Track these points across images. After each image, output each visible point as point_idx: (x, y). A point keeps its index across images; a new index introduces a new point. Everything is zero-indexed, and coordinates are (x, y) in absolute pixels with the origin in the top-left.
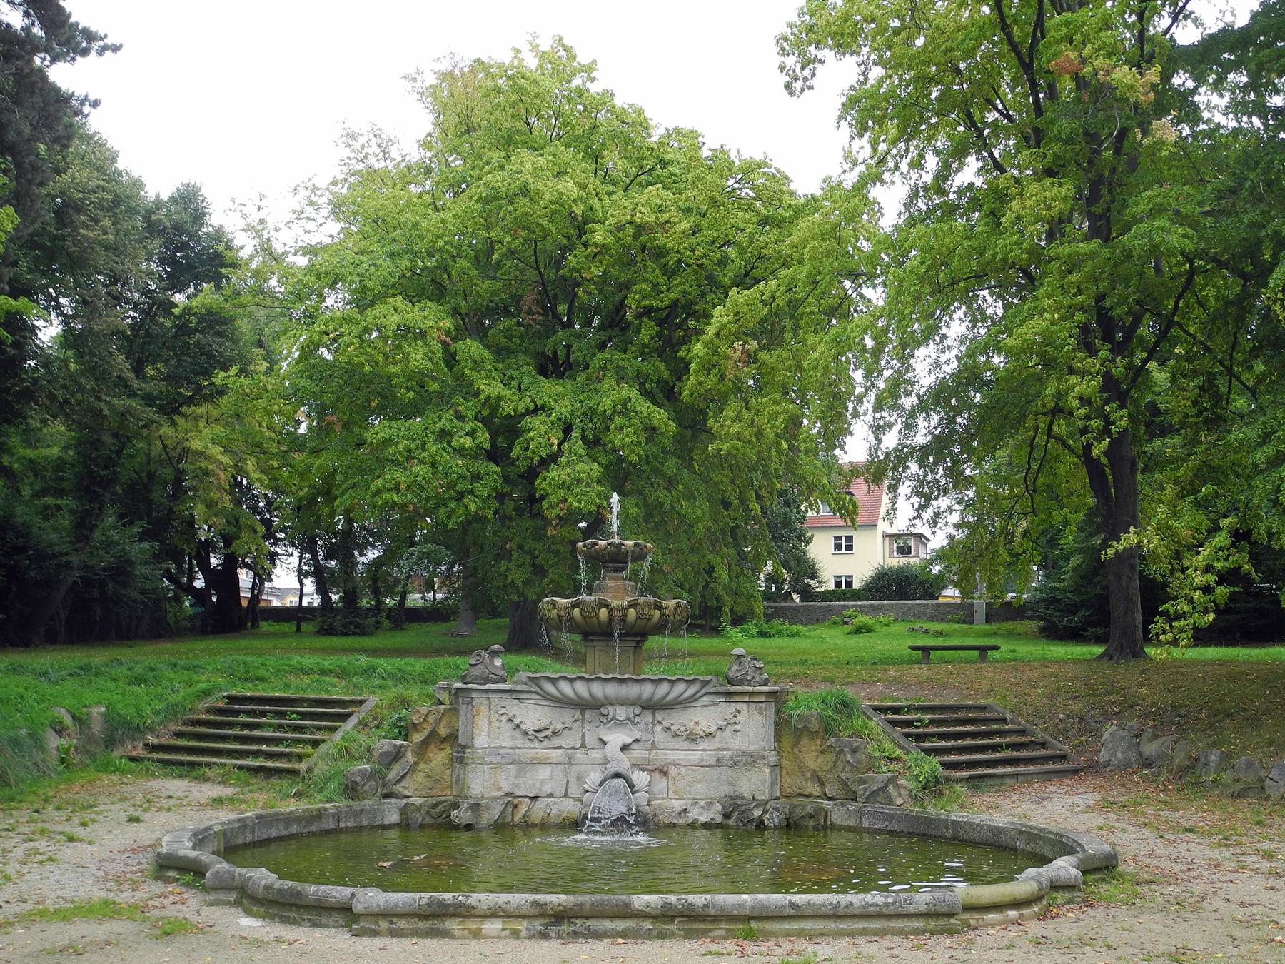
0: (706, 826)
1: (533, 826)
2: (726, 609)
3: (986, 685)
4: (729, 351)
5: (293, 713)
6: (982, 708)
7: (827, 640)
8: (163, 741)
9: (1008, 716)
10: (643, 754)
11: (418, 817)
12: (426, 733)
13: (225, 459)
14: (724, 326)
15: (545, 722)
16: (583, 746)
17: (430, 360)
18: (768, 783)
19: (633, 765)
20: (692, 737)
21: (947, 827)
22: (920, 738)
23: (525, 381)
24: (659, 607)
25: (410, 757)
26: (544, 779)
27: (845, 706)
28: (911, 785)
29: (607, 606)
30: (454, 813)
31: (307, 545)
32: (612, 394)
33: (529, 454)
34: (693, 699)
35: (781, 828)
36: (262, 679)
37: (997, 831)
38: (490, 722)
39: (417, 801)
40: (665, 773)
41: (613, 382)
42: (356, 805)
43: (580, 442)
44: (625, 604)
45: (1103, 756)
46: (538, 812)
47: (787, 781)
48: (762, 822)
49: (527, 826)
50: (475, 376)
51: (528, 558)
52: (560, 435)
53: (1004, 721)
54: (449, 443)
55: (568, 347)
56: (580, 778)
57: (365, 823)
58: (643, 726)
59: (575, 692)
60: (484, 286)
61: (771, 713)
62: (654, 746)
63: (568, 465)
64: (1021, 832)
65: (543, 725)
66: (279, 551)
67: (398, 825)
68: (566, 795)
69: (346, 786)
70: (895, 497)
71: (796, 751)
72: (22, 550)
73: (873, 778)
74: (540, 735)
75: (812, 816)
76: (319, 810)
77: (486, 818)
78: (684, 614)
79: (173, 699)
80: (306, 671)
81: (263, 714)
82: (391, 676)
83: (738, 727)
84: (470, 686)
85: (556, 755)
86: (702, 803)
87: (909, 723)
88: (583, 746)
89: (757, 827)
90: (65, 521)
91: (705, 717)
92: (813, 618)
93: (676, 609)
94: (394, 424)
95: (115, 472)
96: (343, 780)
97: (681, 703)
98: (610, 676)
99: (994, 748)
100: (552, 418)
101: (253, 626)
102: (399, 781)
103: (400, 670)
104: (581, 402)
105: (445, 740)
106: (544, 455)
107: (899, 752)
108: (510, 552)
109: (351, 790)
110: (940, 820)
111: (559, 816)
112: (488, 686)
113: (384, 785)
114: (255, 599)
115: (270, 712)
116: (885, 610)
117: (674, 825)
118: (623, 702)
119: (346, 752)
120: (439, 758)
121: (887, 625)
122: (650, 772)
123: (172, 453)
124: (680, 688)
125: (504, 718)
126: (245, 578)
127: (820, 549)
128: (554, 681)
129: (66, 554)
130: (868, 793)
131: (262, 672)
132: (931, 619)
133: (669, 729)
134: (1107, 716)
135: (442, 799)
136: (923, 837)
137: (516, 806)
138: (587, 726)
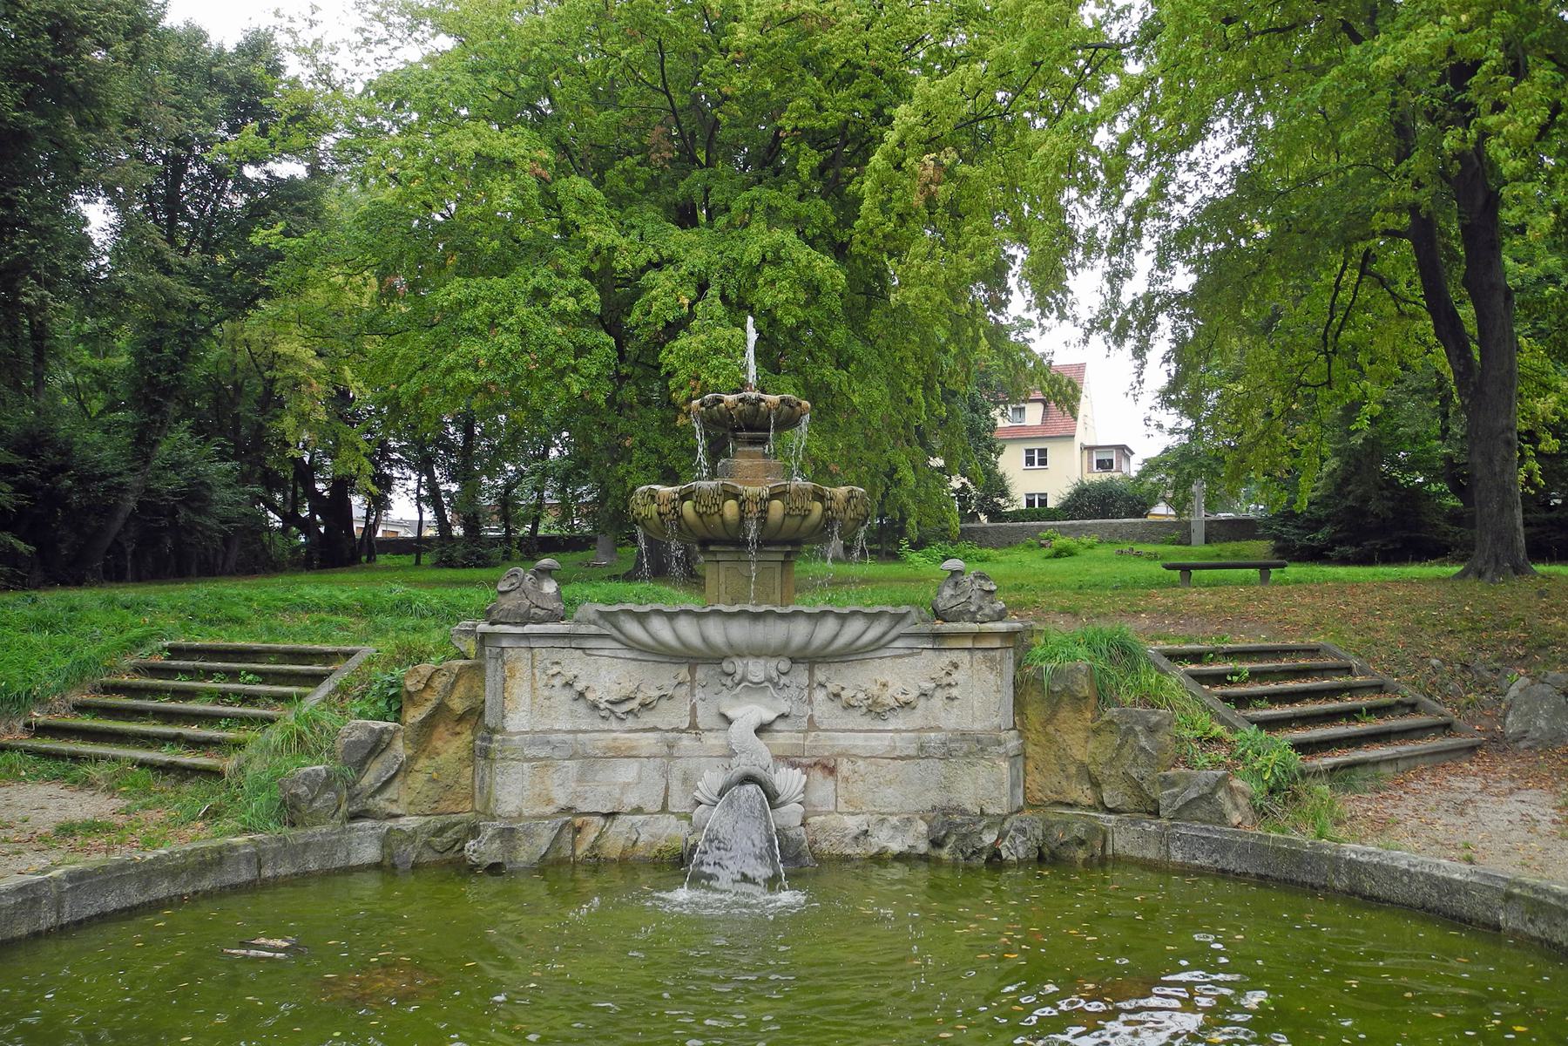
0: (900, 857)
1: (609, 861)
2: (912, 521)
3: (1307, 617)
4: (917, 167)
5: (249, 672)
6: (1313, 652)
7: (1018, 564)
8: (55, 720)
9: (1355, 662)
10: (796, 738)
11: (410, 853)
12: (426, 709)
13: (318, 365)
14: (911, 129)
15: (627, 688)
16: (693, 726)
17: (521, 197)
18: (1007, 785)
19: (777, 758)
20: (876, 710)
21: (1336, 871)
22: (1242, 701)
23: (649, 228)
24: (820, 497)
25: (400, 749)
26: (627, 782)
27: (1124, 652)
28: (1253, 788)
29: (736, 496)
30: (471, 844)
31: (424, 466)
32: (759, 240)
33: (651, 319)
34: (877, 645)
35: (1029, 862)
36: (238, 621)
37: (1449, 887)
38: (533, 689)
39: (409, 823)
40: (831, 771)
41: (763, 226)
42: (296, 835)
43: (718, 302)
44: (765, 493)
45: (1513, 725)
46: (616, 839)
47: (1035, 779)
48: (997, 854)
49: (597, 863)
50: (580, 220)
51: (655, 457)
52: (693, 293)
53: (1348, 670)
54: (545, 305)
55: (707, 190)
56: (688, 780)
57: (313, 866)
58: (793, 692)
59: (678, 637)
60: (600, 119)
61: (1009, 668)
62: (812, 725)
63: (702, 330)
64: (1509, 897)
66: (396, 474)
67: (377, 866)
68: (664, 809)
69: (283, 803)
70: (1142, 365)
71: (1050, 729)
72: (63, 469)
73: (1187, 777)
74: (619, 710)
75: (1081, 843)
76: (219, 850)
77: (526, 853)
78: (861, 509)
79: (90, 651)
80: (307, 608)
81: (209, 674)
82: (435, 613)
83: (954, 692)
84: (498, 628)
85: (648, 741)
86: (894, 820)
87: (1219, 679)
88: (693, 726)
89: (988, 861)
90: (123, 439)
91: (897, 675)
92: (1007, 541)
93: (848, 501)
94: (472, 282)
95: (178, 378)
96: (277, 794)
97: (858, 651)
98: (736, 608)
99: (1351, 715)
100: (682, 271)
101: (369, 560)
102: (380, 790)
103: (449, 605)
104: (721, 253)
105: (461, 719)
106: (670, 318)
107: (1218, 729)
108: (629, 451)
109: (291, 811)
110: (1322, 857)
111: (652, 845)
112: (527, 629)
113: (351, 798)
114: (370, 529)
115: (218, 671)
116: (1089, 530)
117: (847, 859)
118: (758, 652)
119: (299, 743)
120: (451, 747)
121: (1091, 547)
122: (806, 768)
123: (260, 360)
124: (854, 627)
125: (557, 682)
126: (358, 505)
127: (1010, 463)
128: (641, 618)
129: (120, 474)
130: (1179, 803)
131: (241, 611)
132: (1141, 540)
133: (837, 695)
134: (1508, 661)
135: (454, 818)
136: (1290, 885)
137: (578, 830)
138: (699, 693)
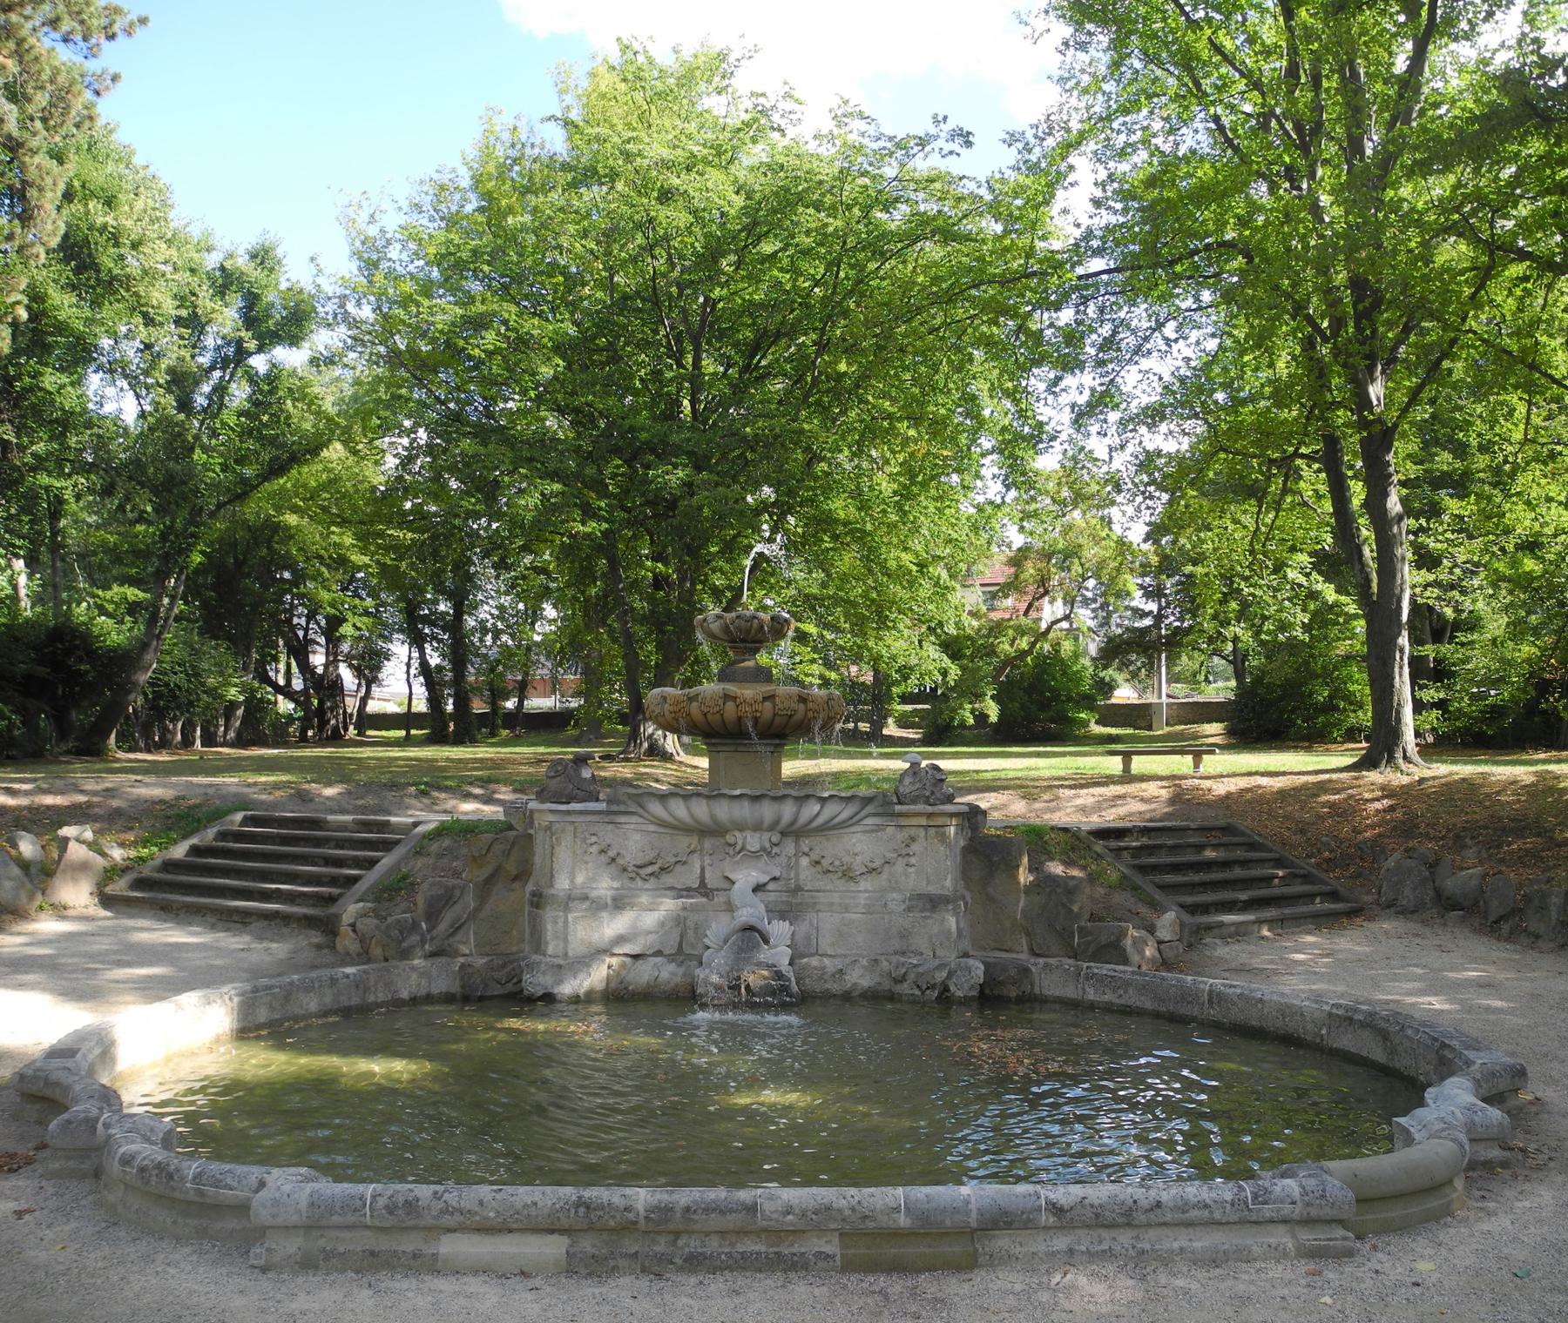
48: (946, 989)
59: (692, 815)
65: (647, 859)
83: (913, 860)
118: (757, 827)
124: (830, 810)
125: (594, 849)
133: (818, 863)
